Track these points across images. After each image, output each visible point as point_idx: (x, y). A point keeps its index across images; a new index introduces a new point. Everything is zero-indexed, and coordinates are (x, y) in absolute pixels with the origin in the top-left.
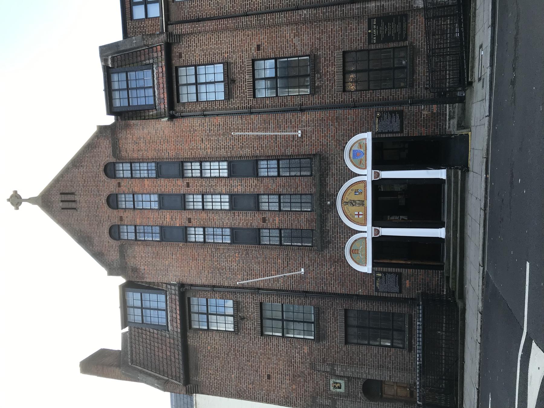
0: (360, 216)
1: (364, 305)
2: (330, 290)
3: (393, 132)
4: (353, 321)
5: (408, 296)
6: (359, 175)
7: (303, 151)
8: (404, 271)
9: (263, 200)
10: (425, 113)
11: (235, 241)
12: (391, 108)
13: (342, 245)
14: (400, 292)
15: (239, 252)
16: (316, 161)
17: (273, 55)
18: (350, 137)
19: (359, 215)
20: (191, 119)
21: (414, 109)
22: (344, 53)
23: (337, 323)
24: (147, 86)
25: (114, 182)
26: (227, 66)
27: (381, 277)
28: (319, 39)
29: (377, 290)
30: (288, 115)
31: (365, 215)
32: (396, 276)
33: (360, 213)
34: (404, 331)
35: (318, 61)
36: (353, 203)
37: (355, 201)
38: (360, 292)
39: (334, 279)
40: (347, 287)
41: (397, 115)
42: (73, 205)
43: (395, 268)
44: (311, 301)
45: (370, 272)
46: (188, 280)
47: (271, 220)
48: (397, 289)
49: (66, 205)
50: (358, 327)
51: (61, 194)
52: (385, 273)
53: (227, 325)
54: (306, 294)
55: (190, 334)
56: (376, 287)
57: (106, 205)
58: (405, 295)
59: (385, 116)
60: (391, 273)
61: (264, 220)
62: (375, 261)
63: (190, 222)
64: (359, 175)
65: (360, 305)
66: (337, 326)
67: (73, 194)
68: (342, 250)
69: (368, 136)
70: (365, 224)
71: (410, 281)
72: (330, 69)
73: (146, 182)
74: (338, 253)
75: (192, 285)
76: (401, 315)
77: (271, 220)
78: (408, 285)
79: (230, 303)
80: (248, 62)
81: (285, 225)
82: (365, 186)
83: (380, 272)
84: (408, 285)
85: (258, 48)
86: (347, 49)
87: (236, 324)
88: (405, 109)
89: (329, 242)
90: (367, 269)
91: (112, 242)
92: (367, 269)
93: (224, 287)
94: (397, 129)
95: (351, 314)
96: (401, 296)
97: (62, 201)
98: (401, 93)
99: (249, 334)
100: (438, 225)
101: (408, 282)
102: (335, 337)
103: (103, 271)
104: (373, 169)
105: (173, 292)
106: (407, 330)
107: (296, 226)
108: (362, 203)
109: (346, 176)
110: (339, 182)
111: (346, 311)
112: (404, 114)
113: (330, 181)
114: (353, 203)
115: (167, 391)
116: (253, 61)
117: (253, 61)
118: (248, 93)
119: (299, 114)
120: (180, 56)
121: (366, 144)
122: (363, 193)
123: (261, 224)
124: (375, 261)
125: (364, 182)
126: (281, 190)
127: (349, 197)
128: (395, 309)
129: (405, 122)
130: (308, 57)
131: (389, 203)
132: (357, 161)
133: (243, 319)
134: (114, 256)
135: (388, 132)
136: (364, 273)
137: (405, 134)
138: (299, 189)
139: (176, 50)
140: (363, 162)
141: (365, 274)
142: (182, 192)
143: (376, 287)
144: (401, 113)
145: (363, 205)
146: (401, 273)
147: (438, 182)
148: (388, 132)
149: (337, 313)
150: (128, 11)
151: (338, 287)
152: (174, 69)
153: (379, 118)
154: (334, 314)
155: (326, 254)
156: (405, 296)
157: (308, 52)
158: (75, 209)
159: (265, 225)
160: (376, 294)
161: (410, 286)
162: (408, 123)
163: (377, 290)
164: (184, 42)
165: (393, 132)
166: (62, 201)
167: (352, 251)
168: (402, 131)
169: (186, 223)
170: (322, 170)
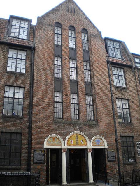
0: (73, 141)
1: (25, 143)
2: (33, 125)
3: (108, 157)
4: (14, 137)
5: (32, 167)
6: (90, 142)
7: (98, 117)
8: (45, 165)
9: (75, 96)
10: (116, 171)
11: (56, 79)
12: (116, 156)
13: (58, 133)
14: (34, 163)
15: (52, 80)
16: (94, 123)
17: (130, 107)
18: (105, 138)
19: (72, 142)
20: (107, 70)
21: (117, 166)
22: (132, 137)
23: (14, 128)
24: (117, 56)
25: (80, 31)
26: (126, 89)
27: (42, 153)
28: (137, 127)
29: (34, 151)
30: (112, 112)
31: (72, 145)
32: (43, 161)
33: (73, 143)
34: (10, 165)
35: (130, 126)
36: (77, 139)
37: (78, 140)
38: (33, 142)
39: (39, 128)
40: (35, 135)
41: (114, 159)
42: (70, 11)
43: (47, 160)
44: (26, 114)
45: (45, 147)
46: (37, 53)
47: (67, 98)
48: (35, 161)
49: (70, 9)
50: (11, 140)
51: (74, 8)
52: (44, 155)
53: (11, 67)
54: (30, 113)
55: (6, 47)
56: (36, 150)
57: (70, 25)
58: (32, 165)
59: (114, 154)
60: (44, 158)
61: (67, 95)
62: (50, 150)
63: (65, 59)
64: (90, 142)
65: (25, 142)
66: (12, 128)
67: (74, 13)
68: (55, 133)
69: (106, 147)
70: (68, 145)
71: (40, 168)
72: (128, 131)
73: (81, 45)
74: (53, 131)
75: (34, 54)
76: (20, 164)
77: (67, 98)
78: (38, 167)
79: (23, 71)
80: (128, 97)
81: (65, 105)
82: (85, 145)
83: (44, 153)
84: (38, 167)
85: (133, 102)
86: (135, 138)
87: (11, 73)
88: (116, 163)
89: (59, 126)
90: (46, 146)
91: (54, 22)
92: (46, 146)
93: (33, 70)
94: (109, 159)
95: (18, 137)
96: (32, 163)
97: (71, 8)
98: (35, 129)
99: (6, 79)
100: (68, 181)
101: (40, 167)
102: (5, 126)
103: (41, 14)
104: (93, 149)
105: (30, 44)
106: (11, 167)
107: (65, 111)
108: (77, 144)
109: (89, 136)
110: (87, 133)
111: (21, 133)
112: (115, 162)
113: (87, 129)
114: (77, 139)
115: (8, 71)
116: (128, 100)
117: (128, 100)
118: (118, 96)
119: (112, 116)
120: (128, 71)
121: (102, 145)
122: (81, 144)
123: (65, 94)
124: (50, 150)
125: (87, 145)
126: (81, 105)
127: (79, 136)
128: (24, 160)
129: (112, 163)
130: (130, 121)
131: (77, 156)
132: (95, 141)
133: (16, 76)
134: (47, 21)
135: (108, 155)
136: (44, 144)
137: (108, 163)
138: (82, 114)
139: (129, 70)
140: (95, 144)
141: (43, 144)
142: (77, 59)
143: (36, 150)
144: (115, 161)
145: (77, 144)
146: (44, 163)
147: (87, 179)
148: (108, 155)
149: (19, 128)
150: (138, 57)
151: (36, 130)
152: (123, 67)
153: (113, 151)
154: (19, 126)
155: (53, 125)
156: (32, 166)
157: (132, 122)
158: (68, 11)
159: (65, 95)
160: (32, 150)
161: (40, 166)
162: (111, 164)
163: (34, 151)
164: (132, 73)
165: (108, 157)
166: (71, 8)
167: (54, 137)
168: (109, 161)
169: (64, 57)
170: (91, 125)
